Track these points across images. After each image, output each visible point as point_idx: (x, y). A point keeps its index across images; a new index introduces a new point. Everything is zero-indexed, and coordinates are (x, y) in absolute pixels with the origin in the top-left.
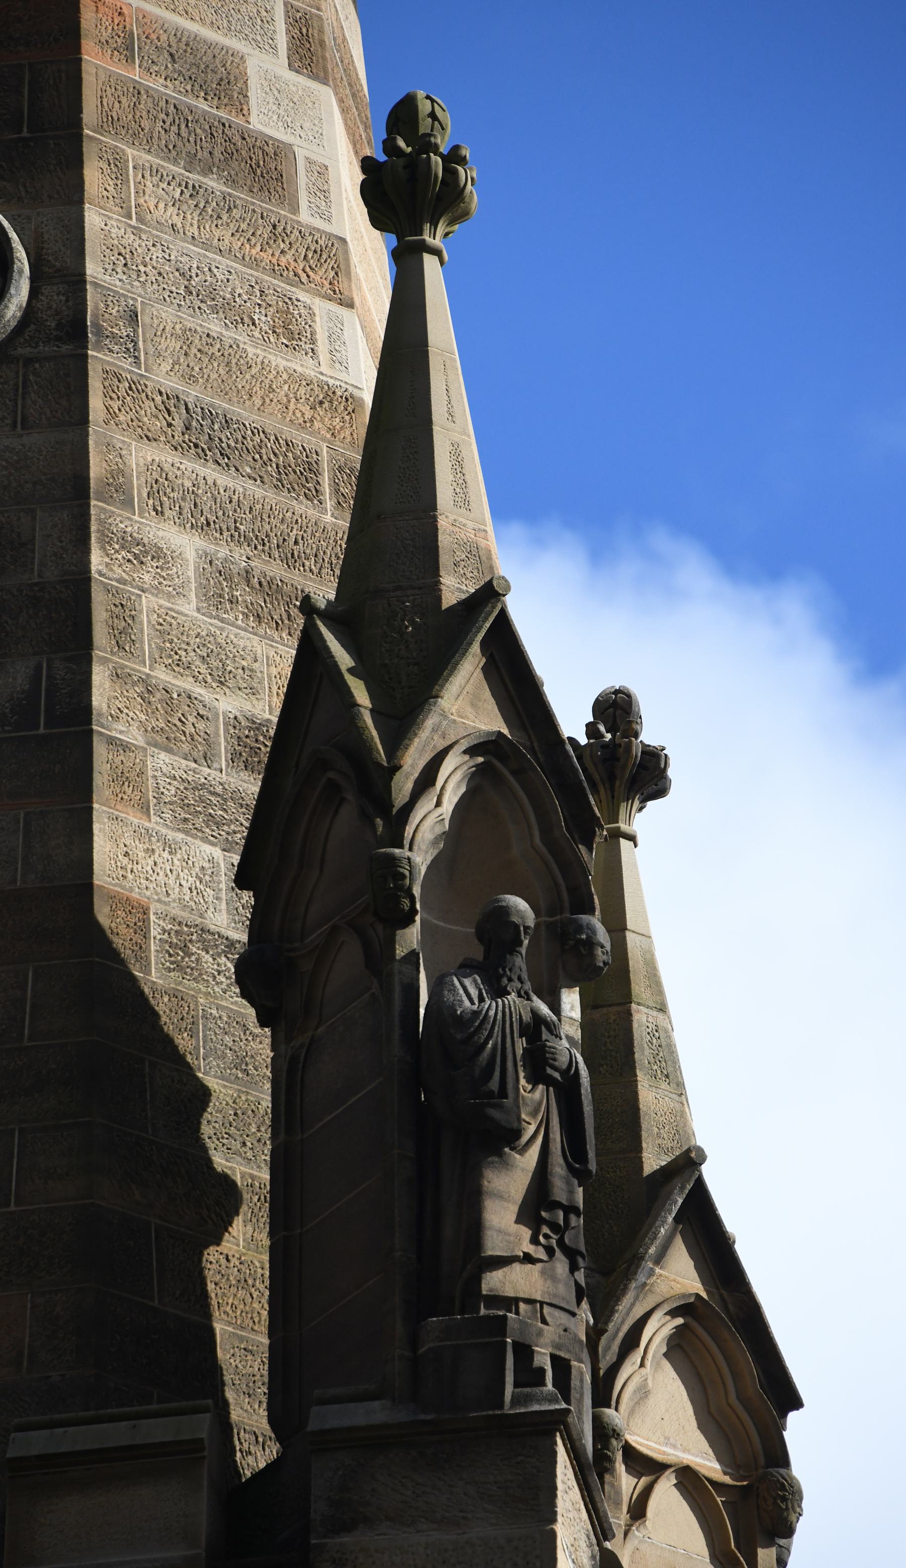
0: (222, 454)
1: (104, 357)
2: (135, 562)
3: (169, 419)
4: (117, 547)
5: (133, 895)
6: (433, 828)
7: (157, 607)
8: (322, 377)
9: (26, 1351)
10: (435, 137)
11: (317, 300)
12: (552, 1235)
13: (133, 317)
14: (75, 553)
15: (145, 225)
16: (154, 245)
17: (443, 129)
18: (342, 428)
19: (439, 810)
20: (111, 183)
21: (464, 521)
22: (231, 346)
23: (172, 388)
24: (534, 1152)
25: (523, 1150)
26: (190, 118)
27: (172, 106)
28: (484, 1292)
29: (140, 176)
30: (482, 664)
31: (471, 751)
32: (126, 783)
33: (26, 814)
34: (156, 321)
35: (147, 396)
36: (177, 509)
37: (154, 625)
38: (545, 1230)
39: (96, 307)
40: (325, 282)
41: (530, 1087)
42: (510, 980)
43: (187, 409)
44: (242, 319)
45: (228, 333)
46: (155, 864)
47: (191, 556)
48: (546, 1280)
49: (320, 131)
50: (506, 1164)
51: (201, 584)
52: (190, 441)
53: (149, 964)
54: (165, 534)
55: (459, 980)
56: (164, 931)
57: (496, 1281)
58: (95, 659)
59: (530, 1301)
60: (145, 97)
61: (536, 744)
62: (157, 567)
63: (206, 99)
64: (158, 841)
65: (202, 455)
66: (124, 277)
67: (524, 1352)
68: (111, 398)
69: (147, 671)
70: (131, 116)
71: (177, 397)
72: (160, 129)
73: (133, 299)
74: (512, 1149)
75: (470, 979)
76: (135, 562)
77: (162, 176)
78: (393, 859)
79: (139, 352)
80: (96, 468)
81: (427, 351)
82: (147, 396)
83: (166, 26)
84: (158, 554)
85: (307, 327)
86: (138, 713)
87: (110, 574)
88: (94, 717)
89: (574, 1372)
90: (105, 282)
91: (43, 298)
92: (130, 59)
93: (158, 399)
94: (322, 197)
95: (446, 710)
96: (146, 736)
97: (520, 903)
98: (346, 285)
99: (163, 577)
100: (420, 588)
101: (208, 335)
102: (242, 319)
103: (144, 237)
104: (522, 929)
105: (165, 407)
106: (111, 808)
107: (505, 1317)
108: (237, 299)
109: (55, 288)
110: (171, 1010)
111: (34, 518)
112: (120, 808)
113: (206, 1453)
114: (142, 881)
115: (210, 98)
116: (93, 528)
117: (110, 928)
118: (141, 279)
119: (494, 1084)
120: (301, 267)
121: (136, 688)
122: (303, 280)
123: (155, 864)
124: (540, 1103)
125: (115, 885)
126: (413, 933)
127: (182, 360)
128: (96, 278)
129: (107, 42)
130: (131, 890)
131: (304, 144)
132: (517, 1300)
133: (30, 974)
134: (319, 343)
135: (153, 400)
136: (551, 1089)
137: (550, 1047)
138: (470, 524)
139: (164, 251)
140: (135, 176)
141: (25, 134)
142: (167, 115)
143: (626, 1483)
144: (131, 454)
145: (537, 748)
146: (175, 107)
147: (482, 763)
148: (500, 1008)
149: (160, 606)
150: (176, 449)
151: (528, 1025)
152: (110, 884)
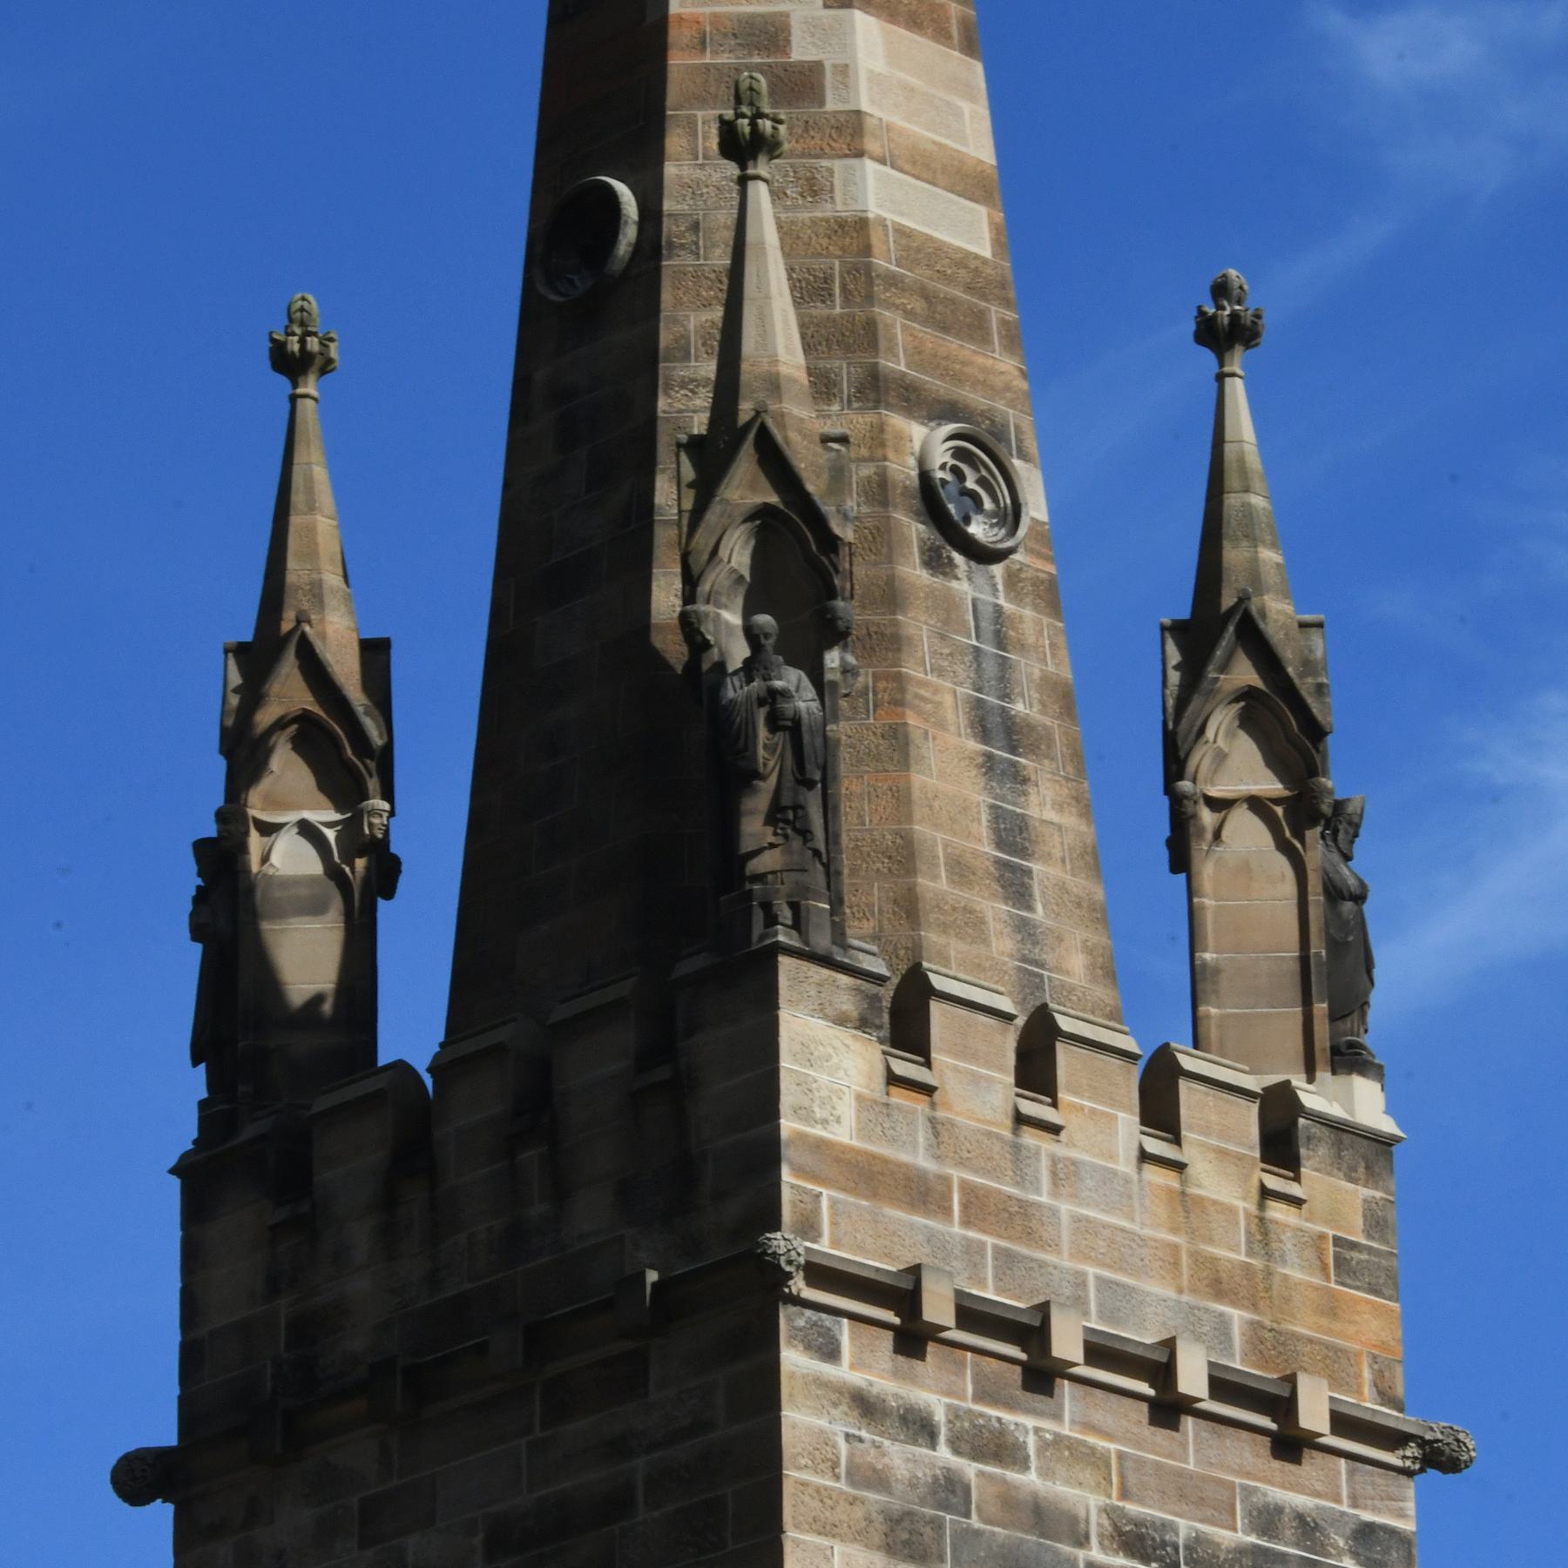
13: (695, 227)
24: (773, 779)
25: (763, 778)
57: (757, 865)
59: (773, 873)
67: (767, 907)
80: (665, 339)
92: (703, 50)
93: (713, 276)
119: (742, 742)
143: (1207, 817)
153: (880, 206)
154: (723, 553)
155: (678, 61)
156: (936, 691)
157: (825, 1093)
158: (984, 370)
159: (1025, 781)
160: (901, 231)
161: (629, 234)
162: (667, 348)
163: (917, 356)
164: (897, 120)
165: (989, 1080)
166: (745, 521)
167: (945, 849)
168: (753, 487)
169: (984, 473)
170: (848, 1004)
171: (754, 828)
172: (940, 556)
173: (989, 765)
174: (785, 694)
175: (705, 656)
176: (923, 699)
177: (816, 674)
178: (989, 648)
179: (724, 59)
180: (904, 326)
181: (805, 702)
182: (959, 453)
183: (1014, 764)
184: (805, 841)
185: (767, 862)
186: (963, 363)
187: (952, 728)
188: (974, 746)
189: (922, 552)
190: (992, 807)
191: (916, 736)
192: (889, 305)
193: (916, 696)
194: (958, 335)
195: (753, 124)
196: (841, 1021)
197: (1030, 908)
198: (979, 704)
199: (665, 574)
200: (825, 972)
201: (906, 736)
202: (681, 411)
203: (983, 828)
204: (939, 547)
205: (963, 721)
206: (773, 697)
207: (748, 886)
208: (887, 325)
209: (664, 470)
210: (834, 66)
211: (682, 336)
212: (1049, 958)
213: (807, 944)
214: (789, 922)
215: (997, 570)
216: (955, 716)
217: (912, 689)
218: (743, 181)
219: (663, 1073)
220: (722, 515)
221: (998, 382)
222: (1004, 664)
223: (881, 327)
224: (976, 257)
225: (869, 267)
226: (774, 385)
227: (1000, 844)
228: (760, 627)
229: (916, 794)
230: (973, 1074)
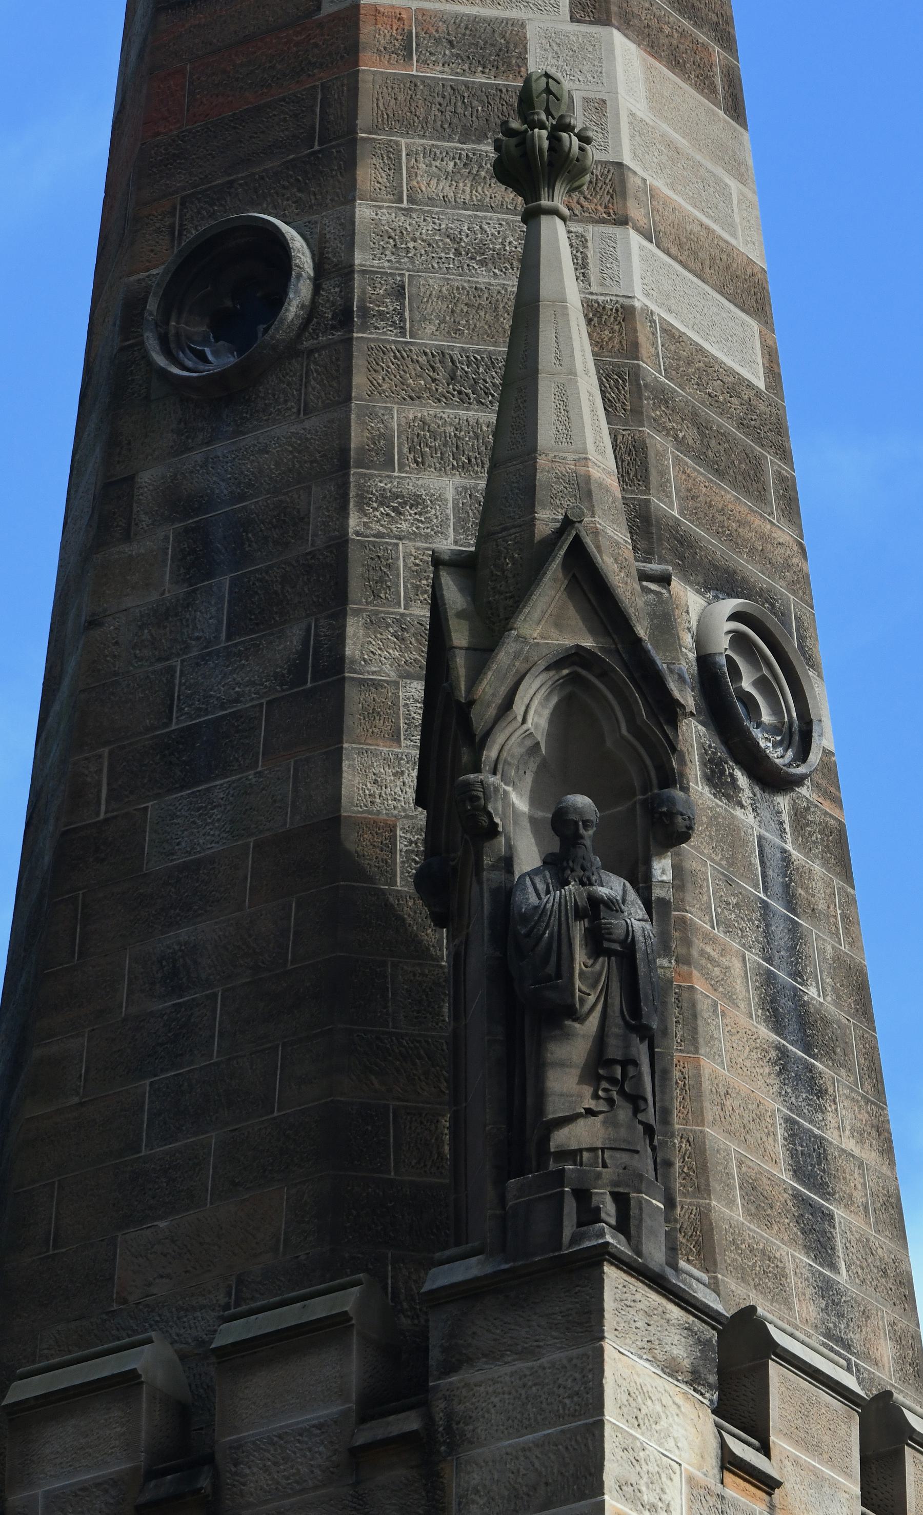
0: (486, 394)
1: (370, 336)
2: (393, 514)
3: (435, 375)
4: (375, 505)
5: (380, 817)
6: (521, 744)
7: (413, 550)
8: (591, 297)
9: (282, 1237)
10: (538, 114)
11: (590, 227)
12: (611, 1088)
13: (399, 292)
14: (338, 519)
15: (416, 204)
16: (425, 220)
17: (558, 100)
18: (610, 339)
19: (525, 727)
20: (384, 175)
21: (564, 455)
22: (499, 292)
23: (436, 346)
24: (593, 1022)
25: (581, 1019)
26: (466, 95)
27: (449, 88)
28: (552, 1150)
29: (413, 160)
30: (564, 586)
31: (555, 665)
32: (377, 718)
33: (296, 762)
34: (422, 290)
35: (412, 360)
36: (439, 455)
37: (410, 568)
38: (605, 1085)
39: (364, 292)
40: (599, 208)
41: (590, 962)
42: (573, 870)
43: (453, 361)
44: (511, 264)
45: (497, 281)
46: (404, 783)
47: (450, 495)
48: (607, 1128)
49: (599, 70)
50: (568, 1035)
51: (460, 518)
52: (454, 390)
53: (395, 875)
54: (425, 481)
55: (531, 879)
56: (411, 842)
57: (562, 1138)
58: (349, 612)
59: (589, 1150)
60: (422, 87)
61: (619, 646)
62: (416, 514)
63: (483, 72)
64: (408, 762)
65: (464, 399)
66: (393, 258)
67: (583, 1196)
68: (375, 371)
69: (402, 610)
70: (407, 108)
71: (442, 353)
72: (437, 113)
73: (400, 275)
74: (574, 1020)
75: (541, 876)
76: (393, 514)
77: (435, 154)
78: (468, 785)
79: (405, 322)
80: (357, 437)
81: (539, 306)
82: (412, 360)
83: (445, 17)
84: (416, 501)
85: (579, 254)
86: (391, 651)
87: (368, 532)
88: (347, 666)
89: (633, 1203)
90: (373, 267)
91: (323, 293)
93: (422, 359)
94: (599, 130)
95: (528, 637)
96: (398, 670)
97: (582, 801)
98: (620, 206)
99: (421, 521)
100: (520, 526)
101: (476, 288)
102: (511, 264)
103: (414, 215)
104: (580, 823)
105: (431, 365)
106: (361, 744)
107: (564, 1169)
108: (507, 248)
109: (332, 282)
110: (415, 913)
111: (310, 493)
112: (370, 742)
113: (353, 1322)
114: (390, 802)
115: (487, 71)
116: (352, 494)
117: (357, 852)
118: (410, 255)
119: (551, 969)
120: (575, 200)
121: (391, 629)
122: (576, 212)
123: (404, 783)
124: (600, 974)
125: (364, 812)
126: (500, 843)
127: (448, 318)
128: (364, 266)
129: (385, 48)
130: (379, 812)
131: (583, 86)
132: (581, 1151)
133: (294, 905)
134: (591, 266)
135: (418, 361)
136: (613, 958)
137: (606, 924)
138: (571, 457)
139: (434, 223)
140: (408, 161)
141: (316, 147)
142: (444, 97)
144: (393, 418)
145: (621, 650)
146: (452, 87)
147: (568, 675)
148: (557, 900)
149: (418, 549)
150: (439, 401)
151: (585, 909)
152: (359, 812)
153: (647, 295)
154: (519, 708)
155: (373, 67)
156: (723, 952)
157: (653, 1468)
158: (763, 537)
159: (821, 1093)
160: (670, 333)
161: (300, 294)
162: (361, 450)
163: (689, 496)
164: (660, 184)
165: (834, 1485)
166: (547, 669)
167: (739, 1167)
168: (558, 624)
169: (765, 672)
170: (680, 1349)
171: (565, 1083)
172: (722, 772)
173: (782, 1062)
174: (612, 905)
175: (487, 847)
176: (710, 959)
177: (641, 881)
178: (778, 907)
179: (436, 73)
180: (676, 458)
181: (635, 918)
182: (738, 639)
183: (810, 1068)
184: (636, 1111)
185: (582, 1134)
186: (741, 523)
187: (742, 1005)
188: (766, 1033)
189: (704, 764)
190: (788, 1120)
191: (704, 1006)
192: (660, 428)
193: (702, 953)
194: (733, 484)
195: (554, 138)
196: (671, 1369)
197: (833, 1267)
198: (769, 979)
199: (360, 752)
200: (655, 1298)
201: (693, 1005)
202: (379, 535)
203: (779, 1149)
204: (721, 761)
205: (754, 999)
206: (595, 909)
207: (552, 1166)
208: (657, 453)
209: (357, 612)
210: (586, 100)
211: (381, 435)
212: (856, 1338)
213: (639, 1253)
214: (613, 1221)
215: (783, 802)
216: (746, 993)
217: (698, 944)
218: (532, 216)
219: (410, 1423)
220: (516, 657)
221: (778, 555)
222: (794, 928)
223: (651, 453)
224: (750, 386)
225: (636, 373)
226: (583, 489)
227: (798, 1172)
228: (576, 810)
229: (706, 1085)
230: (815, 1472)
